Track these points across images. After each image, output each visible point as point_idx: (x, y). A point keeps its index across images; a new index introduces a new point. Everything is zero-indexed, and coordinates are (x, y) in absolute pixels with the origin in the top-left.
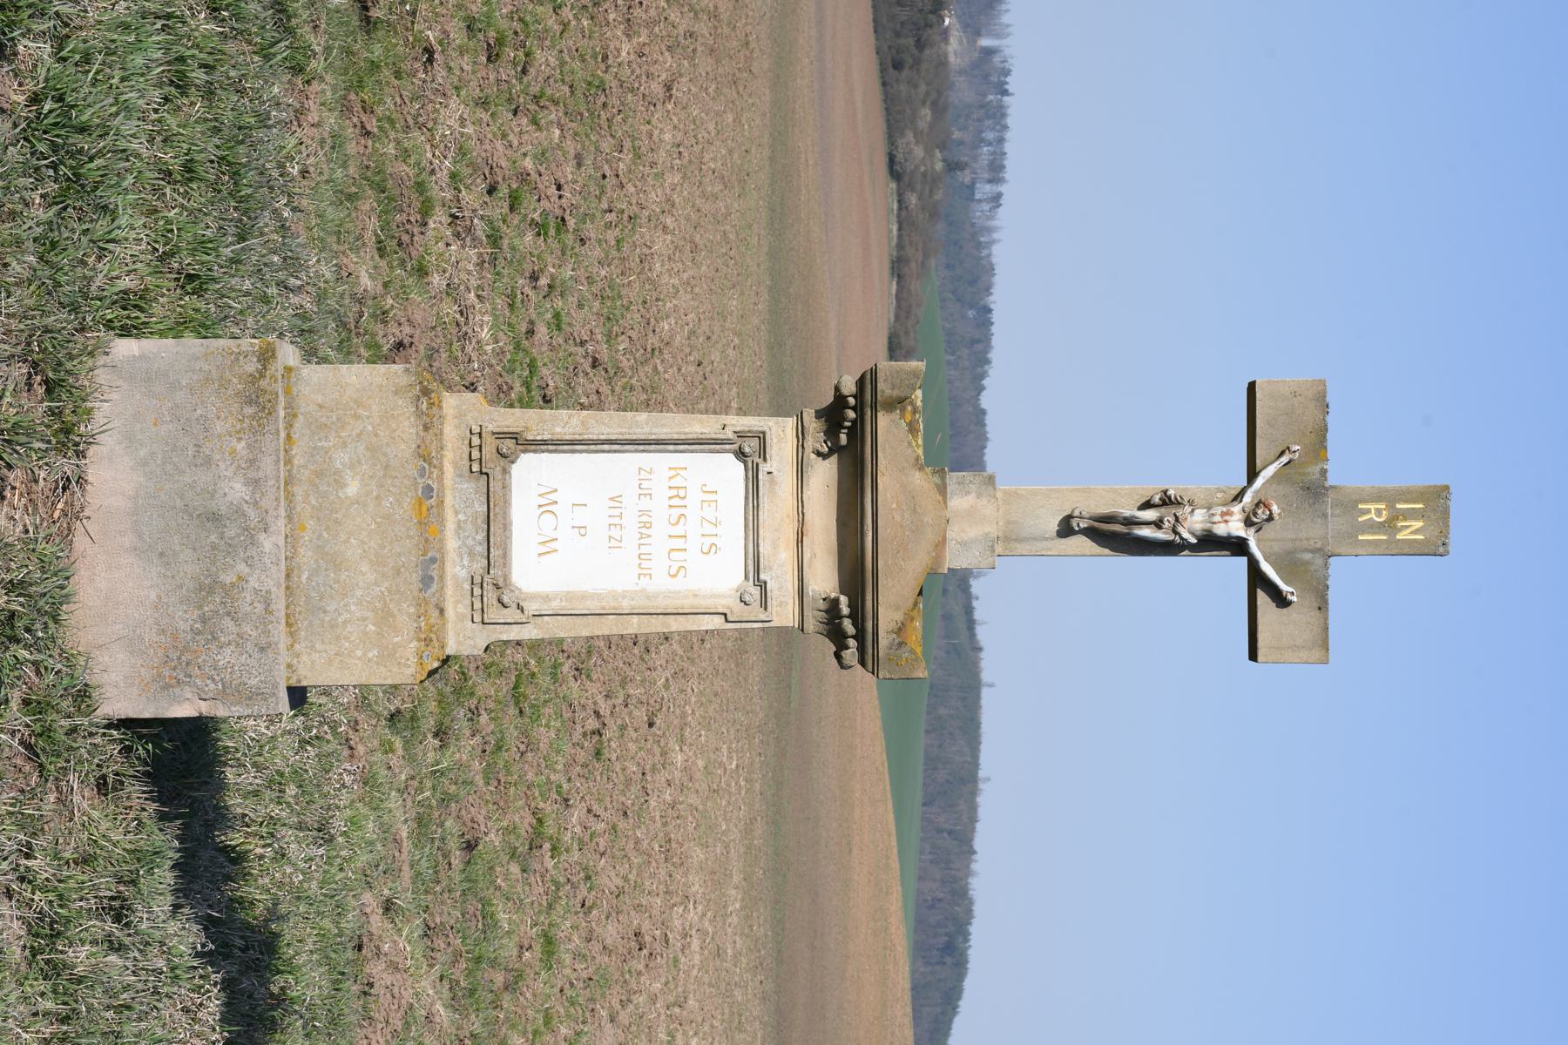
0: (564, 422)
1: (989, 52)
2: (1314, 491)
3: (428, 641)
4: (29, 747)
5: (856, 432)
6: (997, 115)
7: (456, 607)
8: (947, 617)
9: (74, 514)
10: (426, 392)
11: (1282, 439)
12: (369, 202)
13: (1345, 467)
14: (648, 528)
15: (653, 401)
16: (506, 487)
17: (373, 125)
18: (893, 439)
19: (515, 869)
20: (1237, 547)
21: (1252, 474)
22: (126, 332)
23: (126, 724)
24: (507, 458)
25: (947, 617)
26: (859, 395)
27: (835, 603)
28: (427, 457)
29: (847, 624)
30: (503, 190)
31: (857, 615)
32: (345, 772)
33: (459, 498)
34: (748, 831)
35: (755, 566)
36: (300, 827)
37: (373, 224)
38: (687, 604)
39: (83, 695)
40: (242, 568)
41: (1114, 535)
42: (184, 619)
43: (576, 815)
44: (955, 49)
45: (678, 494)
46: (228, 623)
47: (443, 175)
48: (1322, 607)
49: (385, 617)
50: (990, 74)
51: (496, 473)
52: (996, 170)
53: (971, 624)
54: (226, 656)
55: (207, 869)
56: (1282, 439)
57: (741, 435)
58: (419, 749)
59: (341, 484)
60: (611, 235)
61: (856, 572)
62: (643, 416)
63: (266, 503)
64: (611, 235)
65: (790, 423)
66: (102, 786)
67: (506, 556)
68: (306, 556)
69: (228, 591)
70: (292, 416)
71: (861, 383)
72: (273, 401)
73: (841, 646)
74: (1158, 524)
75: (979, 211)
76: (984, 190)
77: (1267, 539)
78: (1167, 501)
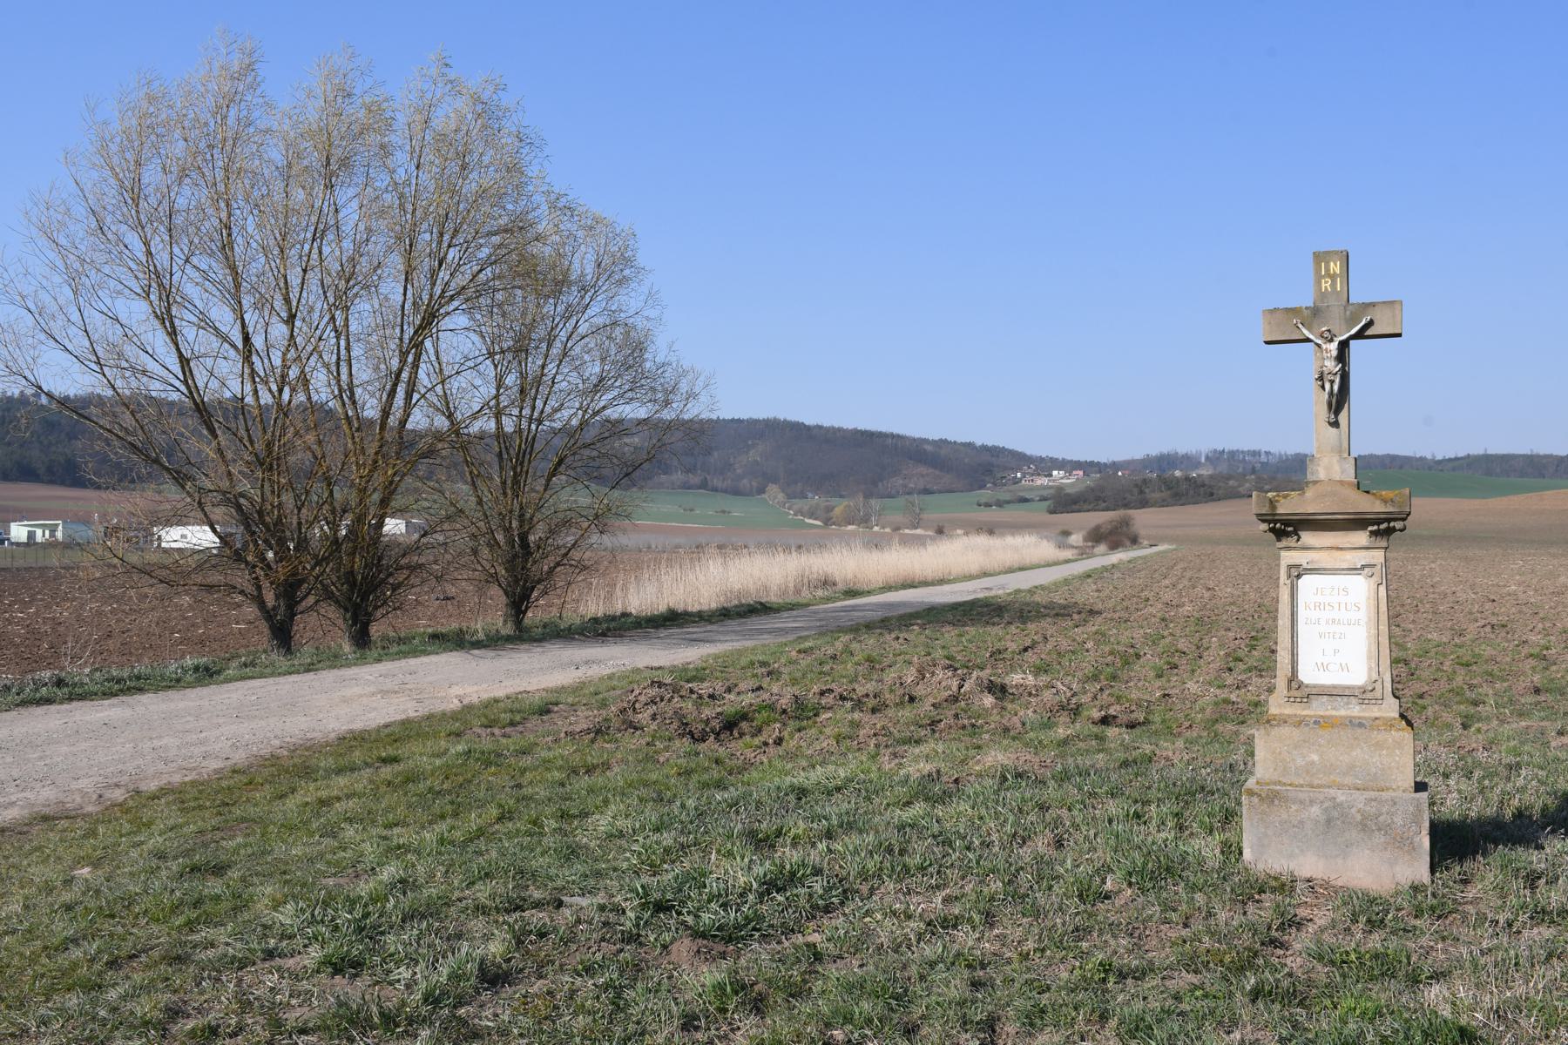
0: (1283, 657)
1: (1207, 458)
2: (1316, 312)
3: (1392, 726)
4: (1439, 917)
5: (1287, 523)
6: (1233, 454)
7: (1375, 712)
8: (1454, 469)
9: (1326, 885)
10: (1268, 721)
11: (1289, 328)
12: (1219, 727)
13: (1306, 300)
14: (1335, 620)
15: (1273, 614)
16: (1315, 686)
17: (1187, 724)
18: (1289, 505)
19: (1554, 668)
20: (1344, 346)
21: (1308, 340)
22: (1241, 853)
23: (1433, 871)
24: (1300, 685)
25: (1454, 469)
26: (1269, 522)
27: (1372, 533)
28: (1300, 722)
29: (1384, 528)
30: (1232, 665)
31: (1378, 522)
32: (1481, 755)
33: (1319, 708)
34: (1554, 556)
35: (1353, 570)
36: (1508, 779)
37: (1229, 726)
38: (1373, 602)
39: (1415, 889)
40: (1353, 810)
41: (1339, 401)
42: (1379, 838)
43: (1533, 638)
44: (1206, 472)
45: (1318, 606)
46: (1381, 819)
47: (1218, 692)
48: (1373, 305)
49: (1379, 746)
50: (1216, 457)
51: (1308, 690)
52: (1256, 454)
53: (1457, 459)
54: (1398, 820)
55: (1518, 830)
56: (1289, 328)
57: (1289, 576)
58: (1484, 714)
59: (1313, 763)
60: (1264, 615)
61: (1356, 523)
62: (1280, 622)
63: (1321, 797)
64: (1264, 615)
65: (1283, 553)
66: (1465, 882)
67: (1348, 687)
68: (1348, 780)
69: (1365, 818)
70: (1280, 783)
71: (1264, 521)
72: (1272, 791)
73: (1394, 530)
74: (1332, 382)
75: (1272, 460)
76: (1263, 458)
77: (1341, 333)
78: (1321, 378)
